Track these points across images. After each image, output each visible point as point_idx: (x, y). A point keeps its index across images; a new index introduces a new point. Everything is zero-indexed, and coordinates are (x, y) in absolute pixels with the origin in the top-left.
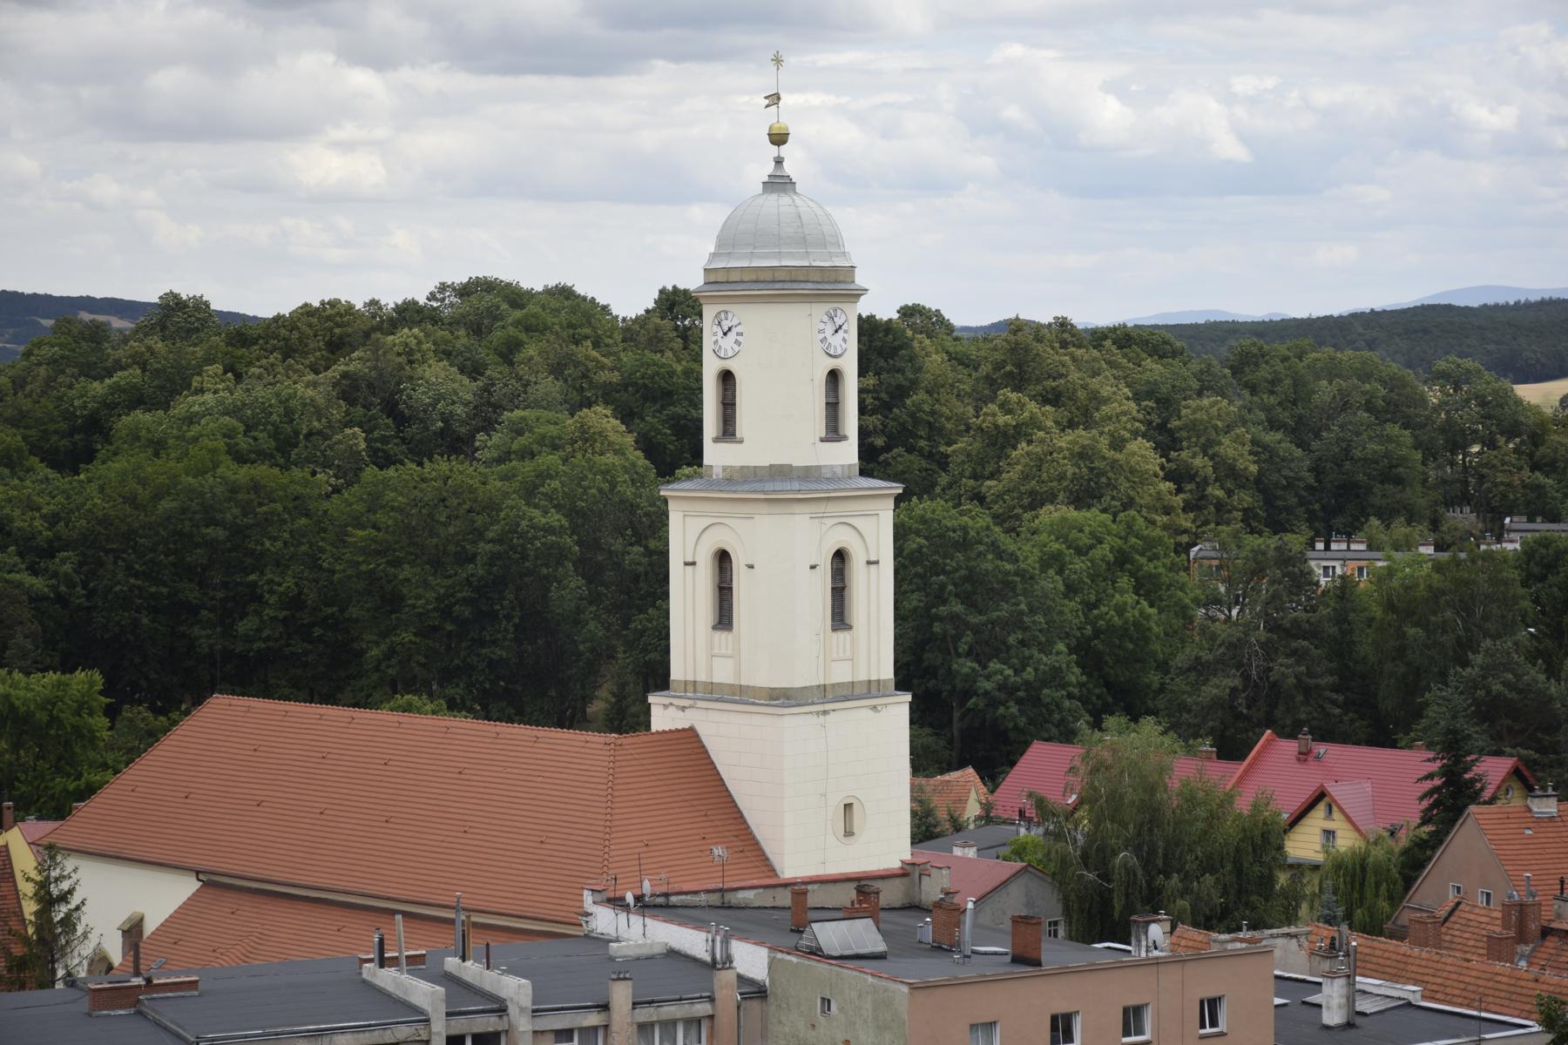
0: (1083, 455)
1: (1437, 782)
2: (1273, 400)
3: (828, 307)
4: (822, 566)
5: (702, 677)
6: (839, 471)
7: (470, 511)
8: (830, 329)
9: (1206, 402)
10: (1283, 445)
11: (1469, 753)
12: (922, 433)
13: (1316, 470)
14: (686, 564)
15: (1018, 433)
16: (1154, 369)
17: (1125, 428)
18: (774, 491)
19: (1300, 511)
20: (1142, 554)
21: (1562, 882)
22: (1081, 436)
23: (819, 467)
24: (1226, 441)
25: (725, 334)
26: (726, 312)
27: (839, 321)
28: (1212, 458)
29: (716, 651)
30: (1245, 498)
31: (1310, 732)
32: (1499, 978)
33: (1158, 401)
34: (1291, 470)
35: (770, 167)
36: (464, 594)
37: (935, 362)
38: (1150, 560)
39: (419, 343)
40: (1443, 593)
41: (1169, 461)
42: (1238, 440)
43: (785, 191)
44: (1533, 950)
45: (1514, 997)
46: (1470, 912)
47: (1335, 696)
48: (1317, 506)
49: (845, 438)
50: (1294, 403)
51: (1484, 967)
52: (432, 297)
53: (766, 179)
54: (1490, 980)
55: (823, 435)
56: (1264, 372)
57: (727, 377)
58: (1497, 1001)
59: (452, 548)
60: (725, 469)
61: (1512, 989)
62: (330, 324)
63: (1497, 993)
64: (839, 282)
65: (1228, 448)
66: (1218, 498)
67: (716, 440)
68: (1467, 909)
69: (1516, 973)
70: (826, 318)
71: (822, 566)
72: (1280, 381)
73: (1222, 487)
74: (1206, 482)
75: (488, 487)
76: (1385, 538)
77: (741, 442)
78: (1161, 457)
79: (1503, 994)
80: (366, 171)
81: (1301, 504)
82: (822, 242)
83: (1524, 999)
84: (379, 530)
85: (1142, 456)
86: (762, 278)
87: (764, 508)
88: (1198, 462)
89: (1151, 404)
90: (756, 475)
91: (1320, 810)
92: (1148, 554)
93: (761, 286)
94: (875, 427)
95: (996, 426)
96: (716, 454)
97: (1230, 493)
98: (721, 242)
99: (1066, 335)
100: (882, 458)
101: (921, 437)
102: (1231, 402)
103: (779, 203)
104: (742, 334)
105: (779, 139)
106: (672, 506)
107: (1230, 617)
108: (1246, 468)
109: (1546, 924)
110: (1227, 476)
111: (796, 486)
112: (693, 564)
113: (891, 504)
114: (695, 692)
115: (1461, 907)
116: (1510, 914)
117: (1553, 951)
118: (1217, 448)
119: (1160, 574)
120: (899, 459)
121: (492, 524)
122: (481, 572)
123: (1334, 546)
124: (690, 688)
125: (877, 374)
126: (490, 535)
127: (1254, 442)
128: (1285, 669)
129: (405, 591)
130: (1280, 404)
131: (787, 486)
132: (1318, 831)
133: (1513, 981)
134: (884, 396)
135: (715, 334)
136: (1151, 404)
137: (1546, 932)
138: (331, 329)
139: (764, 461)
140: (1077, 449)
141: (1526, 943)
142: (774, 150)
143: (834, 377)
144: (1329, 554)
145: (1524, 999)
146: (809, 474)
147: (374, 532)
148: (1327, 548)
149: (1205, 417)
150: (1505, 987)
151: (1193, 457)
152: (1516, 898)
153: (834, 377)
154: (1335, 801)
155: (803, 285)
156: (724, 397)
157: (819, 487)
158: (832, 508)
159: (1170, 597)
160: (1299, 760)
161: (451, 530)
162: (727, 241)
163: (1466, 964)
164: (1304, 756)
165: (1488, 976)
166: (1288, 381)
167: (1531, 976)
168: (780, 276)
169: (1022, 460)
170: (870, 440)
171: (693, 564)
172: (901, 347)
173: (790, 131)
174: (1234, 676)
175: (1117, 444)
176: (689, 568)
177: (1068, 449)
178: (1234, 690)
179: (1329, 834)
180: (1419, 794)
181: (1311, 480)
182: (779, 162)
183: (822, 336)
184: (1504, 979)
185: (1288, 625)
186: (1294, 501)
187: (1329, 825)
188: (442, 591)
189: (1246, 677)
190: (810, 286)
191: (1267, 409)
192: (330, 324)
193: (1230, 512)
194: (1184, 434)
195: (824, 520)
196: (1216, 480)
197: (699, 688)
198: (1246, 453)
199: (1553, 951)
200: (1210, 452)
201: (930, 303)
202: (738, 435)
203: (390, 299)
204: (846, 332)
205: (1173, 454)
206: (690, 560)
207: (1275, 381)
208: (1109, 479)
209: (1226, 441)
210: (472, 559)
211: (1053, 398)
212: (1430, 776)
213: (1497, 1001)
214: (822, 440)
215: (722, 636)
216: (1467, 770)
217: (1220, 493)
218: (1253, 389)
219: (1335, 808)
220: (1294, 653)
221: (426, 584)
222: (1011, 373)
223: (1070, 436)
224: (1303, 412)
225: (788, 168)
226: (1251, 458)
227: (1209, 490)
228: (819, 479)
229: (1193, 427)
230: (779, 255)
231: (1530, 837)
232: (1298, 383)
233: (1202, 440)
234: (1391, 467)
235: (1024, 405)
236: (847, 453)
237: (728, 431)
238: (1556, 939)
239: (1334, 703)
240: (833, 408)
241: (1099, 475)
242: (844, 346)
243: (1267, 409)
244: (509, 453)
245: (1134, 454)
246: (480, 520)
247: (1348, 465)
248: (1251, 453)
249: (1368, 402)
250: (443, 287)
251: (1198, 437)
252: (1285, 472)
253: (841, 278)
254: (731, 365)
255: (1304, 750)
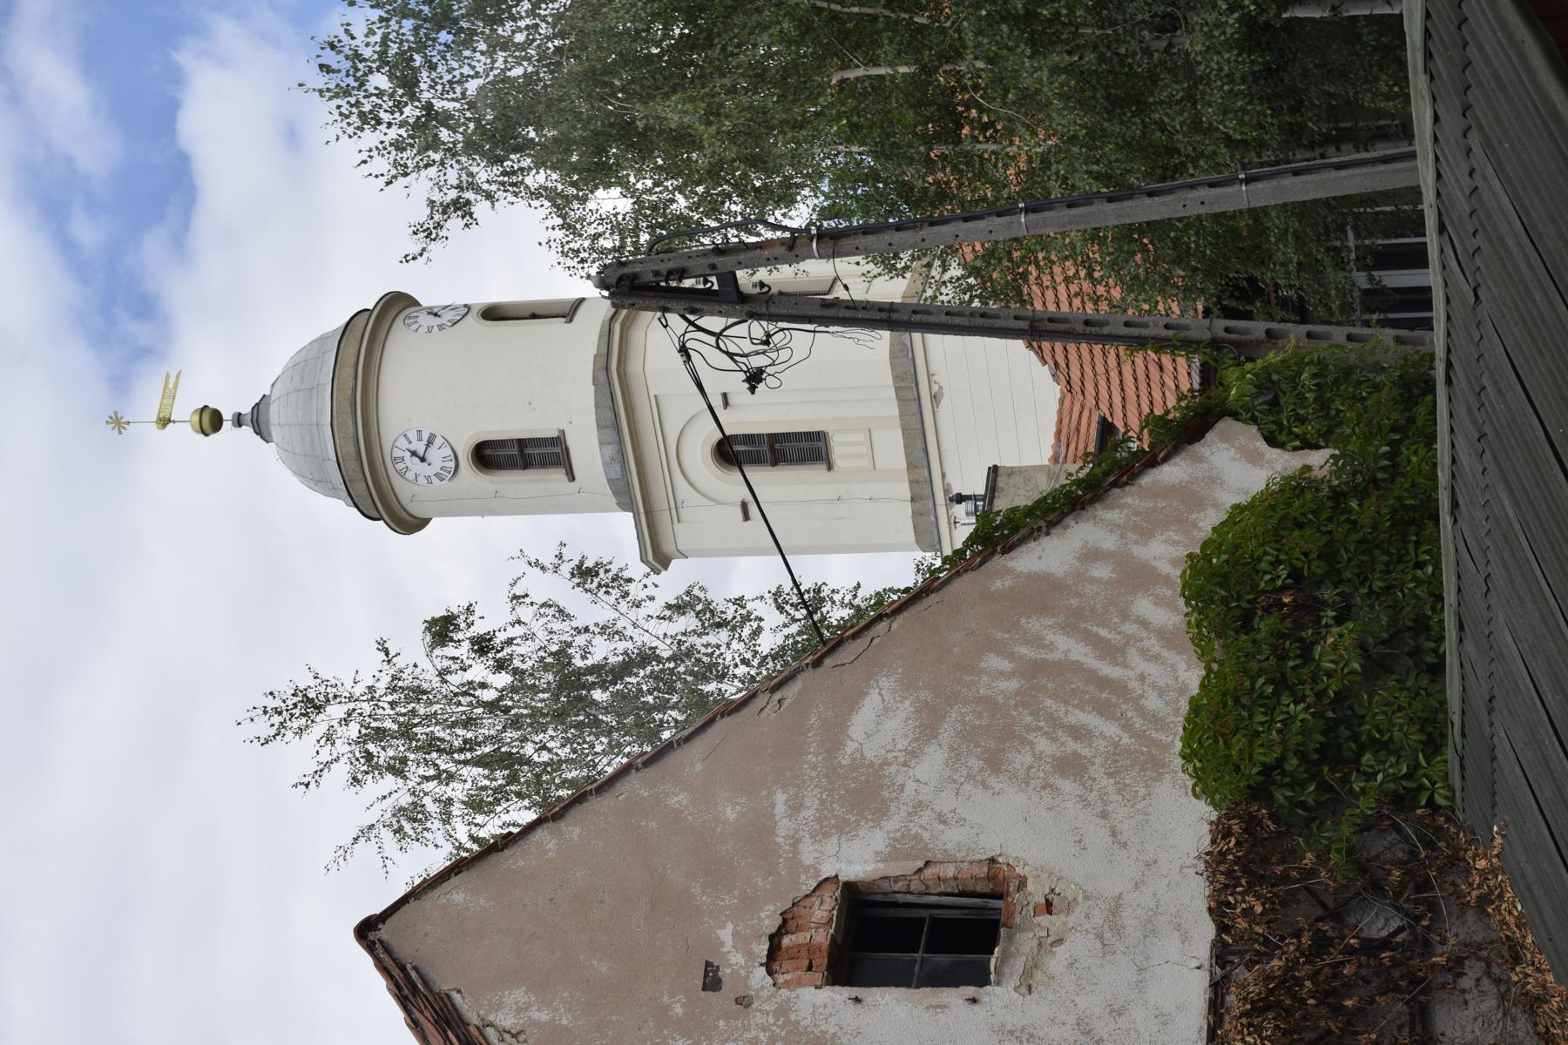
103: (275, 415)
104: (419, 432)
105: (212, 421)
142: (227, 425)
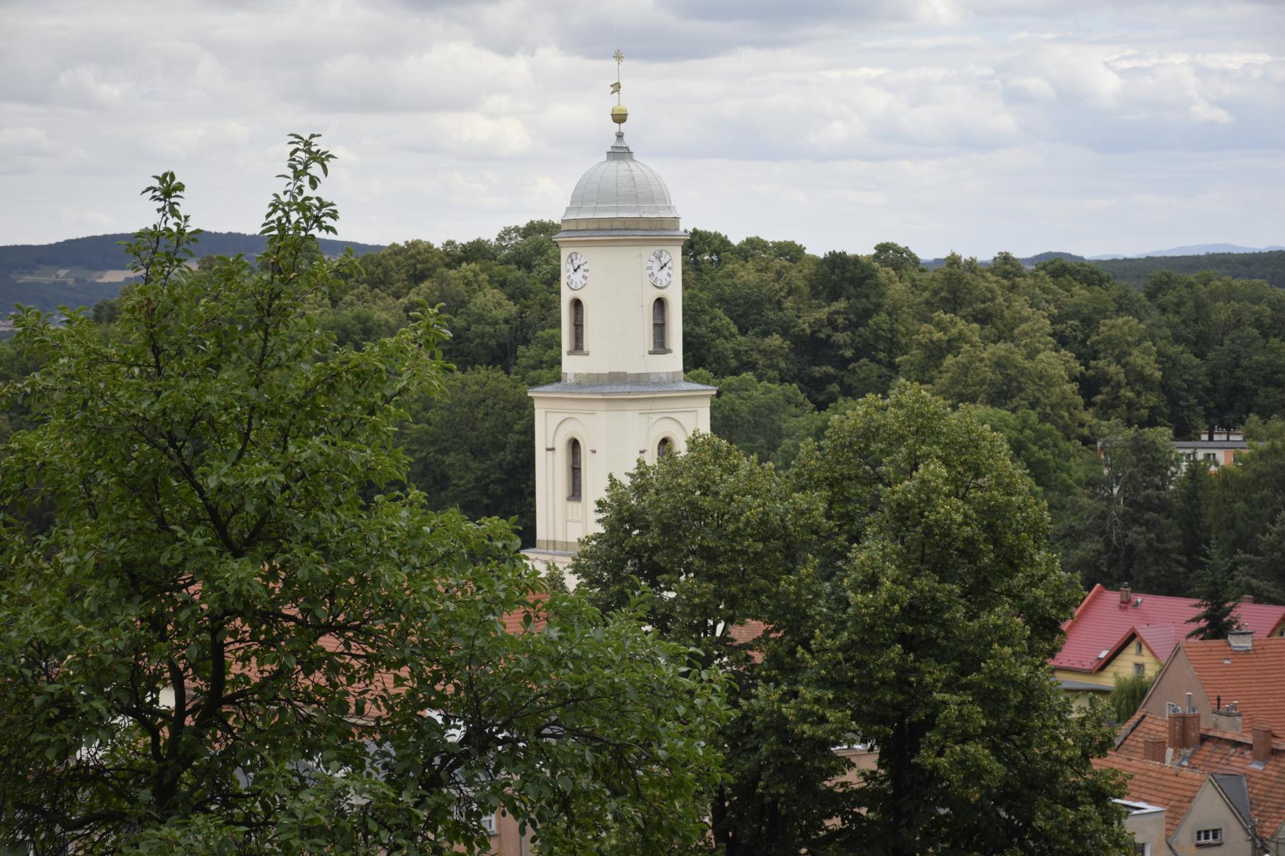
0: (999, 364)
1: (1203, 624)
2: (1177, 319)
3: (656, 249)
4: (650, 451)
5: (560, 538)
6: (665, 378)
7: (503, 409)
8: (657, 266)
9: (1120, 321)
10: (1185, 356)
11: (1227, 601)
12: (882, 347)
13: (1213, 376)
14: (548, 450)
15: (951, 346)
16: (1081, 294)
17: (1039, 342)
18: (610, 393)
19: (1200, 409)
20: (1035, 444)
21: (1219, 700)
22: (1002, 348)
23: (648, 374)
24: (1135, 352)
25: (575, 270)
26: (576, 254)
27: (664, 260)
28: (1124, 366)
29: (570, 518)
30: (1152, 399)
31: (1129, 586)
32: (1150, 773)
33: (1083, 321)
34: (1191, 375)
35: (613, 140)
36: (497, 475)
37: (898, 289)
38: (1041, 448)
39: (476, 275)
40: (1264, 475)
41: (1087, 369)
42: (1146, 352)
43: (623, 159)
44: (1194, 753)
45: (1160, 788)
46: (1152, 723)
47: (1180, 558)
48: (1212, 404)
49: (669, 351)
50: (1196, 321)
51: (1140, 765)
52: (501, 238)
53: (610, 150)
54: (1144, 775)
55: (651, 348)
56: (1170, 297)
57: (577, 304)
58: (1148, 791)
59: (489, 438)
60: (576, 375)
61: (1159, 782)
62: (413, 261)
63: (1148, 785)
64: (664, 230)
65: (1137, 358)
66: (1129, 398)
67: (570, 353)
68: (1150, 720)
69: (1163, 770)
70: (653, 258)
71: (650, 451)
72: (1185, 303)
73: (1132, 390)
74: (1119, 386)
75: (518, 390)
76: (1264, 431)
77: (587, 354)
78: (1081, 365)
79: (1152, 786)
80: (514, 135)
81: (1200, 403)
82: (651, 199)
83: (1167, 790)
84: (430, 424)
85: (1049, 364)
86: (602, 227)
87: (602, 406)
88: (1113, 369)
89: (1076, 323)
90: (598, 380)
91: (1132, 648)
92: (1040, 443)
93: (602, 233)
94: (845, 342)
95: (931, 341)
96: (571, 365)
97: (1139, 394)
98: (574, 199)
99: (1008, 267)
100: (850, 367)
101: (881, 350)
102: (1141, 321)
103: (620, 168)
105: (620, 118)
106: (537, 404)
107: (1112, 494)
108: (1152, 375)
109: (1205, 732)
110: (1137, 380)
111: (628, 388)
112: (553, 449)
113: (708, 403)
114: (554, 549)
115: (1146, 719)
116: (1175, 725)
117: (1208, 754)
118: (1128, 358)
119: (1049, 460)
120: (865, 368)
121: (519, 419)
122: (509, 458)
123: (1216, 437)
124: (551, 546)
125: (848, 298)
126: (517, 427)
127: (1160, 353)
128: (1137, 535)
129: (450, 473)
130: (1183, 322)
131: (621, 389)
132: (1131, 665)
133: (1160, 776)
134: (852, 316)
135: (568, 271)
136: (1076, 323)
137: (1204, 739)
138: (414, 265)
139: (604, 369)
140: (994, 359)
141: (1188, 747)
143: (660, 304)
144: (1211, 444)
145: (1167, 790)
146: (639, 380)
147: (427, 426)
148: (1211, 439)
149: (1119, 334)
150: (1155, 781)
151: (1109, 366)
152: (1180, 712)
153: (660, 304)
154: (1143, 640)
155: (634, 233)
156: (576, 320)
157: (646, 389)
158: (657, 406)
159: (1056, 478)
160: (1120, 607)
161: (487, 424)
162: (578, 199)
163: (1128, 763)
164: (1125, 604)
165: (1143, 772)
166: (1190, 303)
167: (1173, 772)
168: (616, 225)
169: (952, 369)
170: (841, 352)
171: (553, 449)
172: (867, 278)
173: (629, 112)
174: (1098, 541)
175: (1031, 355)
176: (550, 453)
177: (989, 359)
178: (1099, 553)
179: (1139, 667)
180: (1188, 633)
181: (1208, 383)
182: (620, 136)
183: (650, 272)
184: (1154, 774)
185: (1142, 501)
186: (1193, 401)
187: (1139, 660)
188: (479, 473)
189: (1108, 542)
190: (640, 233)
191: (1172, 326)
192: (413, 261)
193: (1138, 409)
194: (1101, 346)
195: (651, 416)
196: (1128, 384)
197: (558, 546)
198: (1152, 363)
199: (1208, 754)
200: (1123, 362)
201: (884, 242)
202: (585, 349)
203: (464, 237)
204: (670, 268)
205: (1092, 363)
206: (550, 446)
207: (1180, 304)
208: (1020, 383)
209: (1135, 352)
210: (503, 448)
211: (983, 318)
212: (1197, 620)
213: (1148, 791)
214: (650, 353)
215: (573, 506)
216: (1227, 613)
217: (1130, 394)
218: (1164, 310)
219: (1144, 647)
220: (1147, 523)
221: (467, 467)
222: (946, 299)
223: (991, 348)
224: (1202, 328)
225: (627, 141)
226: (1156, 366)
227: (1122, 391)
228: (646, 384)
229: (1109, 341)
230: (617, 209)
231: (1228, 666)
232: (1199, 306)
233: (1117, 351)
234: (1275, 373)
235: (956, 323)
236: (674, 361)
237: (578, 347)
238: (1211, 744)
239: (1179, 563)
240: (660, 328)
241: (1011, 381)
242: (668, 279)
243: (1172, 326)
244: (542, 362)
245: (1042, 361)
246: (510, 416)
247: (1239, 373)
248: (1156, 362)
249: (1257, 320)
250: (507, 232)
251: (1113, 349)
252: (1186, 377)
253: (666, 226)
254: (580, 295)
255: (1125, 600)
